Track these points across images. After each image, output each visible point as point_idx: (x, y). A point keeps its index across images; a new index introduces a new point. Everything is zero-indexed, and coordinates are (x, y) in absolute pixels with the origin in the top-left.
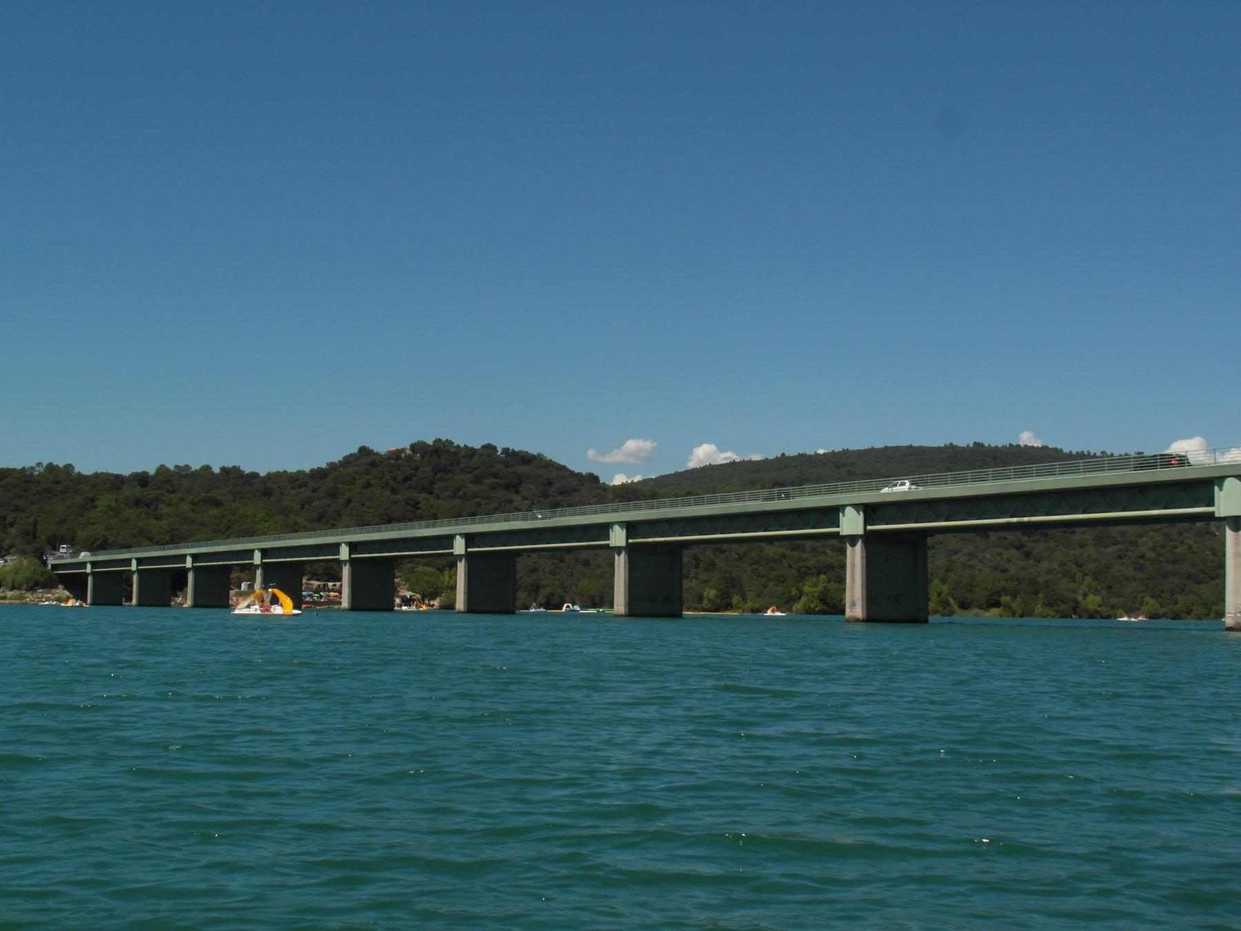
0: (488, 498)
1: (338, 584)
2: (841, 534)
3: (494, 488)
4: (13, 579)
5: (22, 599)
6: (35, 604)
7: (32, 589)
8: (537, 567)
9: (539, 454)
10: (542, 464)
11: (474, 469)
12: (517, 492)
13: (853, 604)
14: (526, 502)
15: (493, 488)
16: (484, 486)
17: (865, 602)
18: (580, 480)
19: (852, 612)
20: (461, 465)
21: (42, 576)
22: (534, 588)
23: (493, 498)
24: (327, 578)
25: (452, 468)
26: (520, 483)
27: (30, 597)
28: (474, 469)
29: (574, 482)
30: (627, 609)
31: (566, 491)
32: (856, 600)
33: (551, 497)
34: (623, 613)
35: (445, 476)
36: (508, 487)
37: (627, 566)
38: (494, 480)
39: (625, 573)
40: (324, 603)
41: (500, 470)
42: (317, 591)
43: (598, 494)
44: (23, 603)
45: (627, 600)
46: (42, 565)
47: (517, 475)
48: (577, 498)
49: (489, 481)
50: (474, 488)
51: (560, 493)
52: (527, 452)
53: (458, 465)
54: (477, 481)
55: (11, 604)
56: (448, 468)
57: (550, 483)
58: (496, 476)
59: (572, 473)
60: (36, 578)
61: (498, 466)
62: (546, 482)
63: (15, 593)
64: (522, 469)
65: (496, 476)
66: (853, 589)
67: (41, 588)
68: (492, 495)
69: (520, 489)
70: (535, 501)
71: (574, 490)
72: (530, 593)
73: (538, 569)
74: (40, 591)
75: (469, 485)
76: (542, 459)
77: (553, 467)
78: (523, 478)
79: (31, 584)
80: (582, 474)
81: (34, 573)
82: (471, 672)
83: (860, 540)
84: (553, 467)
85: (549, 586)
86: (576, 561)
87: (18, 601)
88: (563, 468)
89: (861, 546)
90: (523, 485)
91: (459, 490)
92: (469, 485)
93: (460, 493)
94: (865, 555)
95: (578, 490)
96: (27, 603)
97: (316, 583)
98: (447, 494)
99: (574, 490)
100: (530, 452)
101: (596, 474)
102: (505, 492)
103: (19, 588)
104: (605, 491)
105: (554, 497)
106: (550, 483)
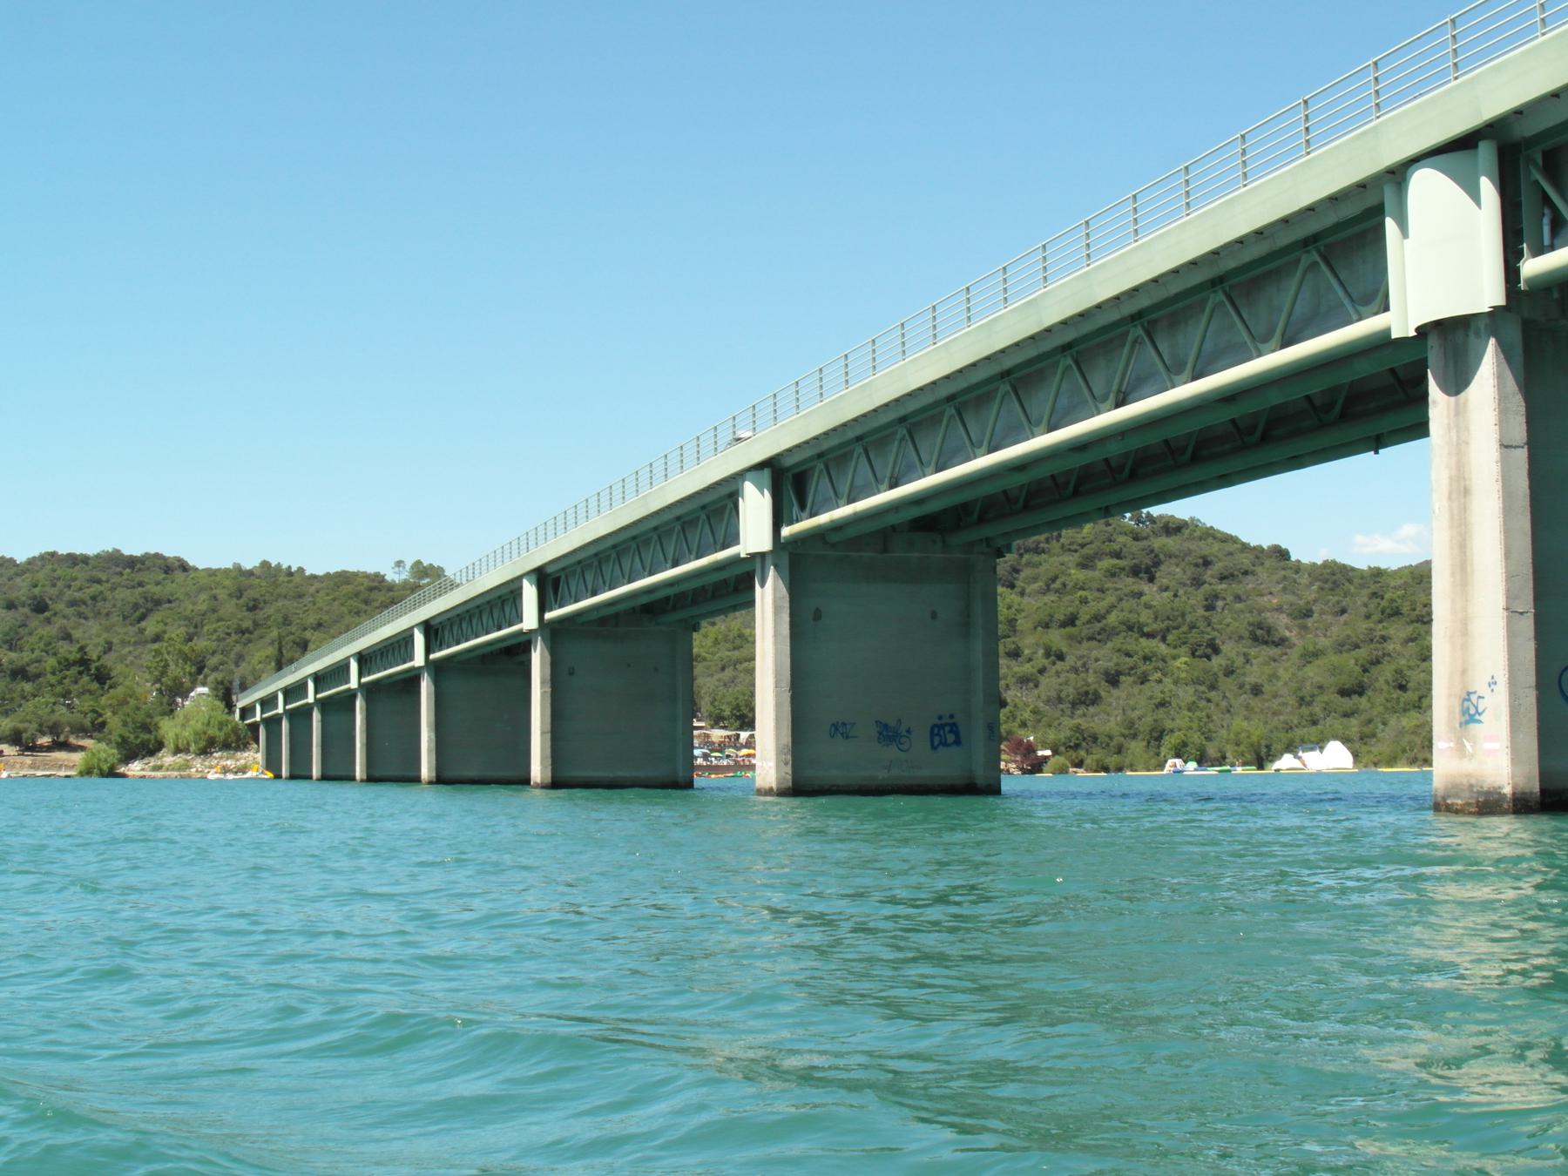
0: (1101, 590)
1: (744, 735)
2: (1394, 335)
3: (1113, 575)
4: (176, 735)
5: (185, 770)
6: (202, 778)
7: (205, 752)
8: (1168, 699)
9: (1192, 519)
10: (1197, 534)
11: (1083, 546)
12: (1152, 579)
13: (1469, 715)
14: (1165, 594)
15: (1112, 574)
16: (1097, 573)
17: (1530, 699)
18: (1257, 557)
19: (1460, 750)
20: (1062, 540)
21: (220, 729)
22: (1155, 734)
23: (1108, 590)
24: (738, 724)
25: (1046, 546)
26: (1157, 564)
27: (198, 764)
28: (1083, 546)
29: (1245, 560)
30: (789, 769)
31: (1232, 575)
32: (1479, 685)
33: (1206, 585)
34: (774, 786)
35: (1036, 558)
36: (1135, 572)
37: (786, 618)
38: (1115, 561)
39: (776, 643)
40: (728, 768)
41: (1125, 546)
42: (721, 747)
43: (1285, 578)
44: (182, 777)
45: (787, 739)
46: (226, 711)
47: (1152, 551)
48: (1251, 586)
49: (1106, 563)
50: (1078, 575)
51: (1223, 578)
52: (1172, 516)
53: (1058, 541)
54: (1086, 564)
55: (165, 777)
56: (1042, 545)
57: (1207, 563)
58: (1117, 555)
59: (1245, 547)
60: (211, 732)
61: (1122, 539)
62: (1200, 561)
63: (180, 759)
64: (1159, 542)
65: (1117, 555)
66: (1463, 629)
67: (220, 750)
68: (1108, 585)
69: (1157, 575)
70: (1181, 592)
71: (1246, 573)
72: (1149, 742)
73: (1170, 703)
74: (220, 753)
75: (1073, 571)
76: (1197, 526)
77: (1215, 538)
78: (1162, 556)
79: (202, 744)
80: (1261, 547)
81: (208, 724)
82: (530, 959)
83: (1492, 341)
84: (1215, 538)
85: (1180, 730)
86: (1240, 688)
87: (176, 773)
88: (1228, 539)
89: (1500, 377)
90: (1163, 567)
91: (1054, 579)
92: (1073, 571)
93: (1057, 585)
94: (1519, 432)
95: (1253, 573)
96: (189, 777)
97: (717, 734)
98: (1036, 586)
99: (1246, 573)
100: (1177, 516)
101: (1283, 547)
102: (1131, 580)
103: (187, 751)
104: (1297, 572)
105: (1210, 584)
106: (1207, 563)
